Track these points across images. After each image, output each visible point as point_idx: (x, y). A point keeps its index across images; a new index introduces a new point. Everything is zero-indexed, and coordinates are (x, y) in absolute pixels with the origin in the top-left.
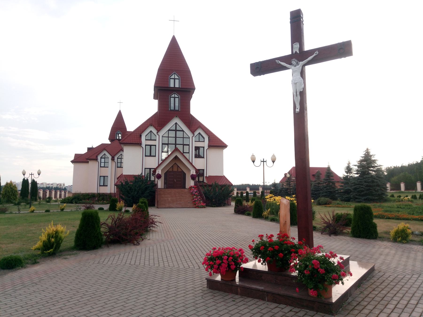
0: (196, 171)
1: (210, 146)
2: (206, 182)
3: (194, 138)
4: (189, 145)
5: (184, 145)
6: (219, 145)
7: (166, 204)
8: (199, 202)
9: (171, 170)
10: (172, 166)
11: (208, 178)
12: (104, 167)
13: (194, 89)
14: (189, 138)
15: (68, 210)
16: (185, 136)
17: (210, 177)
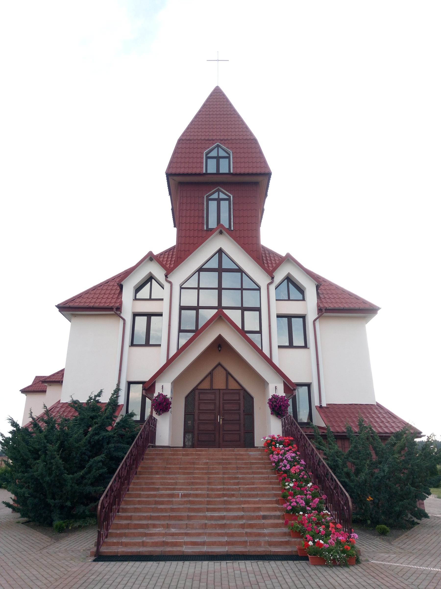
0: (285, 385)
2: (323, 425)
3: (272, 288)
4: (259, 309)
6: (352, 306)
7: (154, 526)
8: (314, 515)
9: (206, 385)
10: (211, 374)
11: (326, 410)
13: (268, 175)
14: (259, 289)
15: (144, 475)
16: (247, 284)
17: (331, 407)
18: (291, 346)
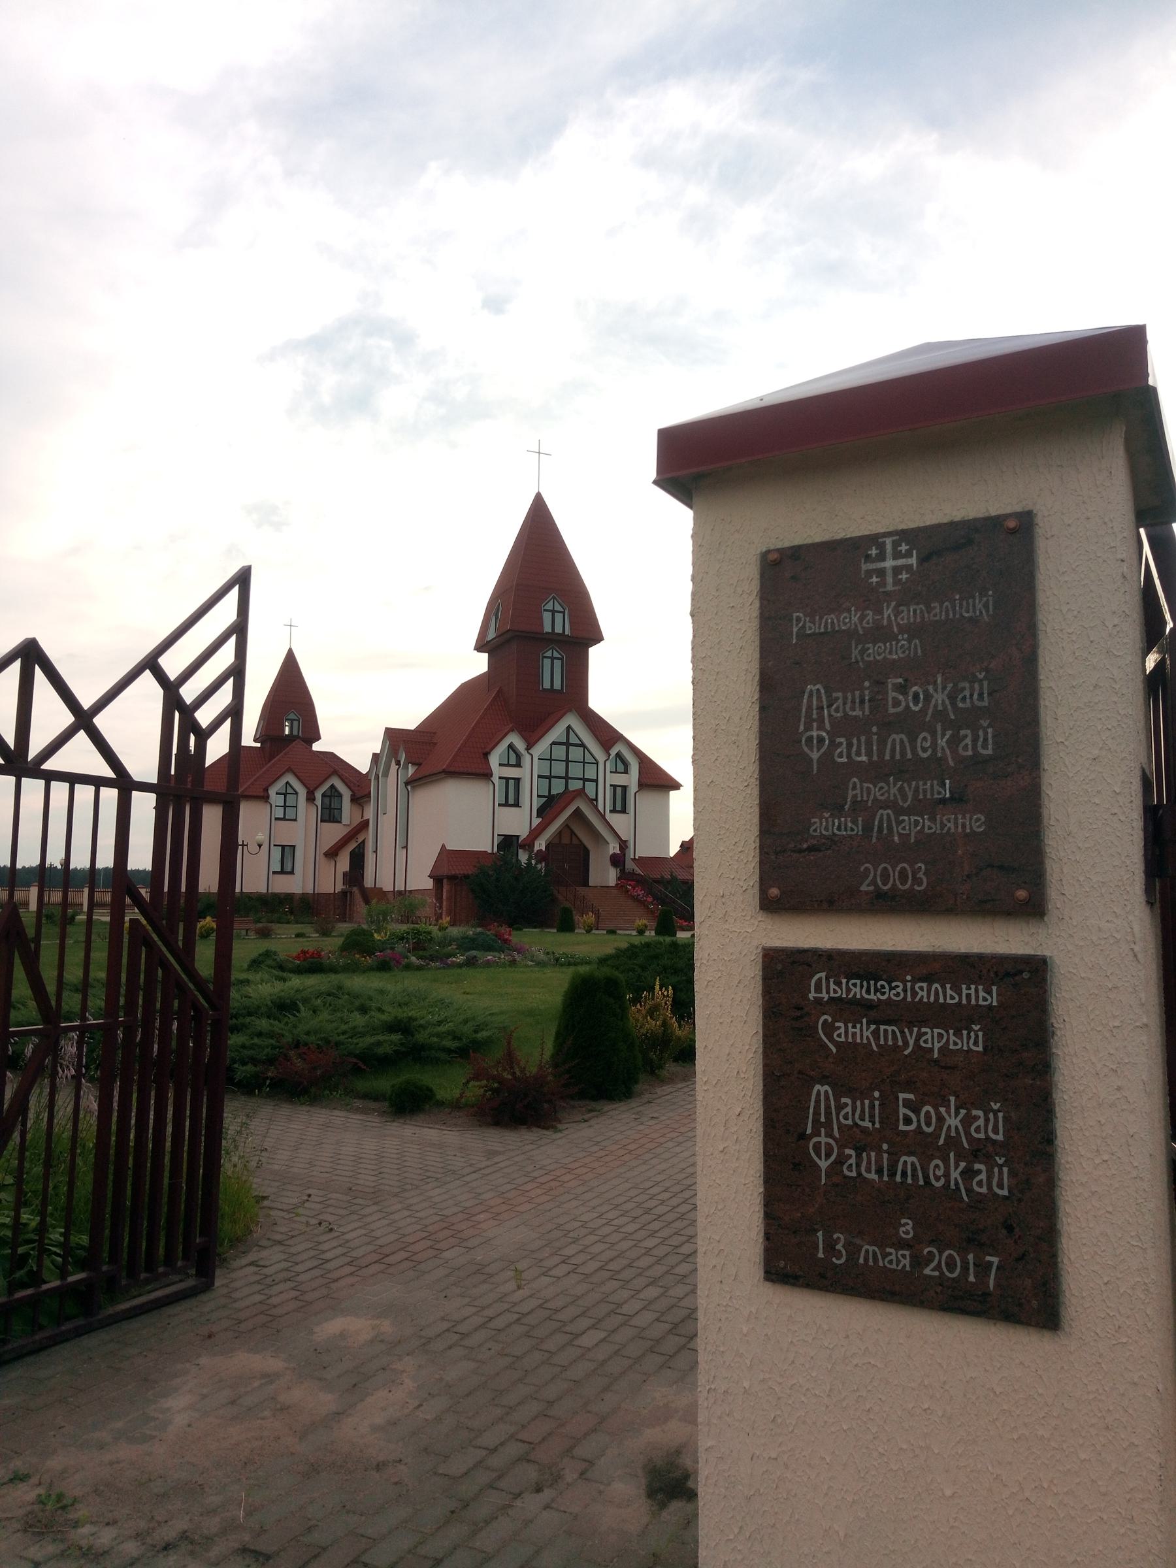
1: (642, 785)
4: (596, 781)
5: (585, 780)
12: (284, 819)
14: (597, 763)
16: (588, 758)
18: (616, 772)
